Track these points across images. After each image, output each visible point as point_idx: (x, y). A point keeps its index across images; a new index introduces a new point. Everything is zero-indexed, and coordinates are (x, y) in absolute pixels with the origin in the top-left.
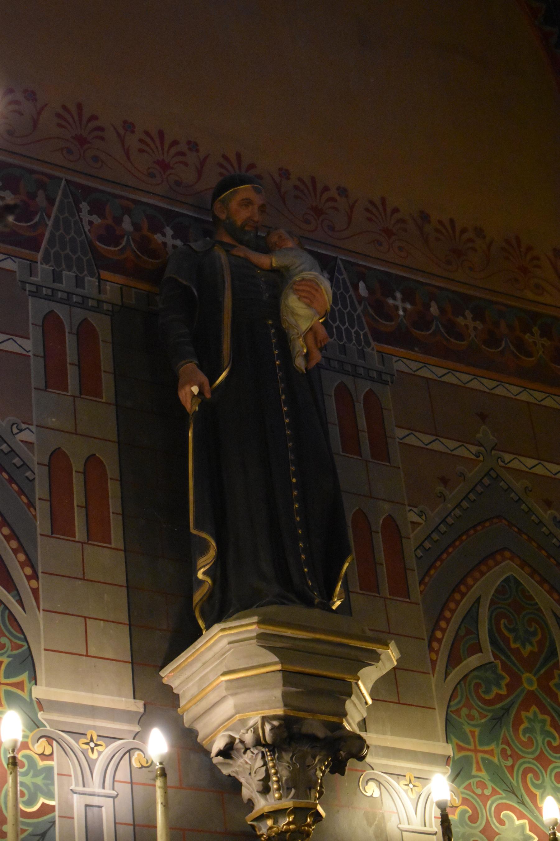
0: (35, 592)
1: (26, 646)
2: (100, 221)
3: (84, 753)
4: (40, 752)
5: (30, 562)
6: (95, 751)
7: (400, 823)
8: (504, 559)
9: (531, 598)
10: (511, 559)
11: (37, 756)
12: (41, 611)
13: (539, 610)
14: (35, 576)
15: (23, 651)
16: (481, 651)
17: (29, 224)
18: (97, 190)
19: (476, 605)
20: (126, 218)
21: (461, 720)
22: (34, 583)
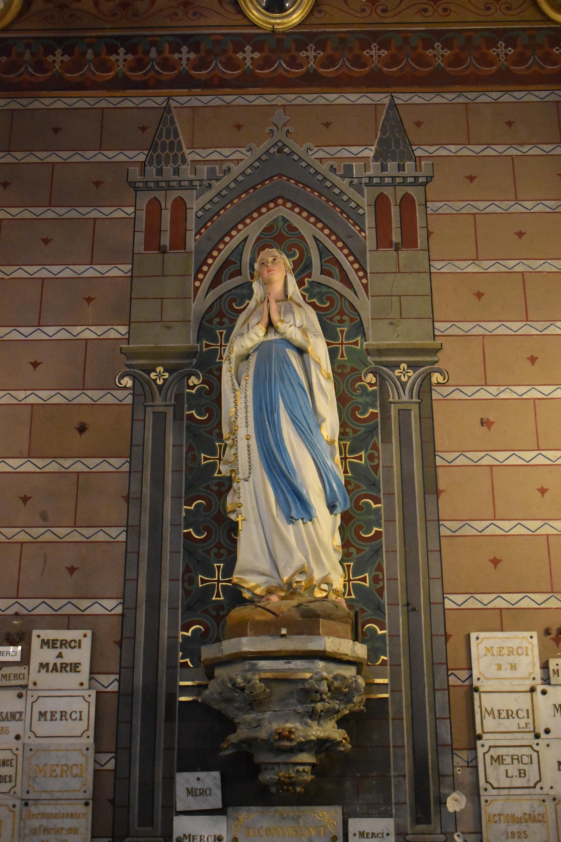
0: (365, 286)
1: (359, 320)
2: (449, 52)
3: (399, 378)
4: (368, 382)
5: (362, 268)
6: (406, 376)
7: (145, 402)
8: (277, 205)
9: (296, 229)
10: (284, 205)
11: (368, 385)
12: (370, 297)
13: (302, 238)
14: (365, 276)
15: (357, 323)
16: (241, 275)
17: (271, 70)
18: (194, 35)
19: (243, 243)
20: (153, 49)
21: (334, 324)
22: (364, 281)
